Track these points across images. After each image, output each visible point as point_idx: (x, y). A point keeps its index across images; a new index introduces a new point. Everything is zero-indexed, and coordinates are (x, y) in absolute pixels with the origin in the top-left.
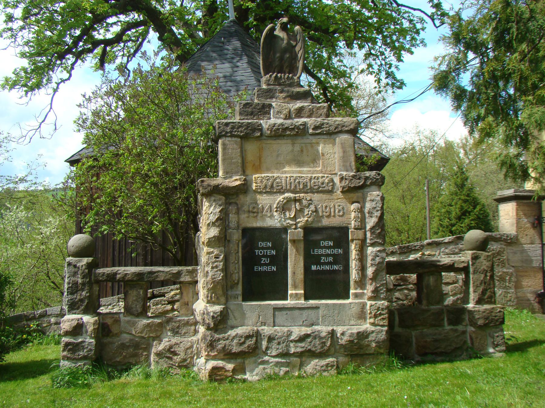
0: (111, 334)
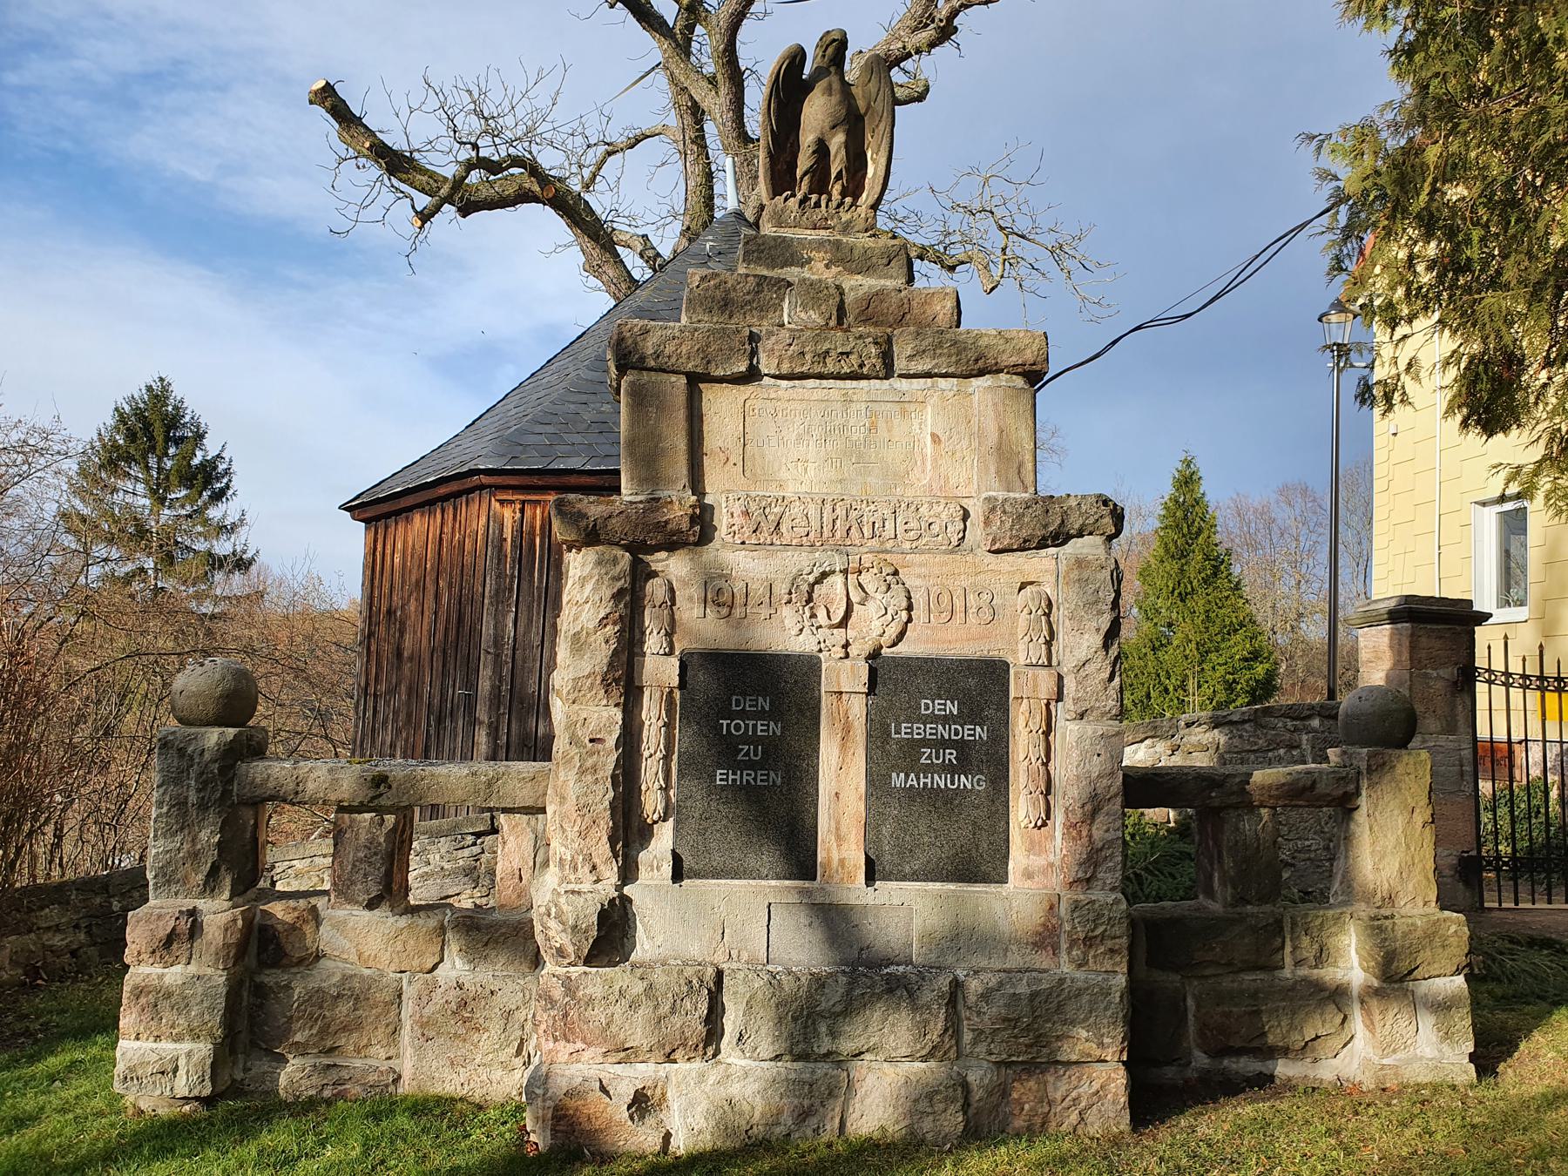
0: (284, 961)
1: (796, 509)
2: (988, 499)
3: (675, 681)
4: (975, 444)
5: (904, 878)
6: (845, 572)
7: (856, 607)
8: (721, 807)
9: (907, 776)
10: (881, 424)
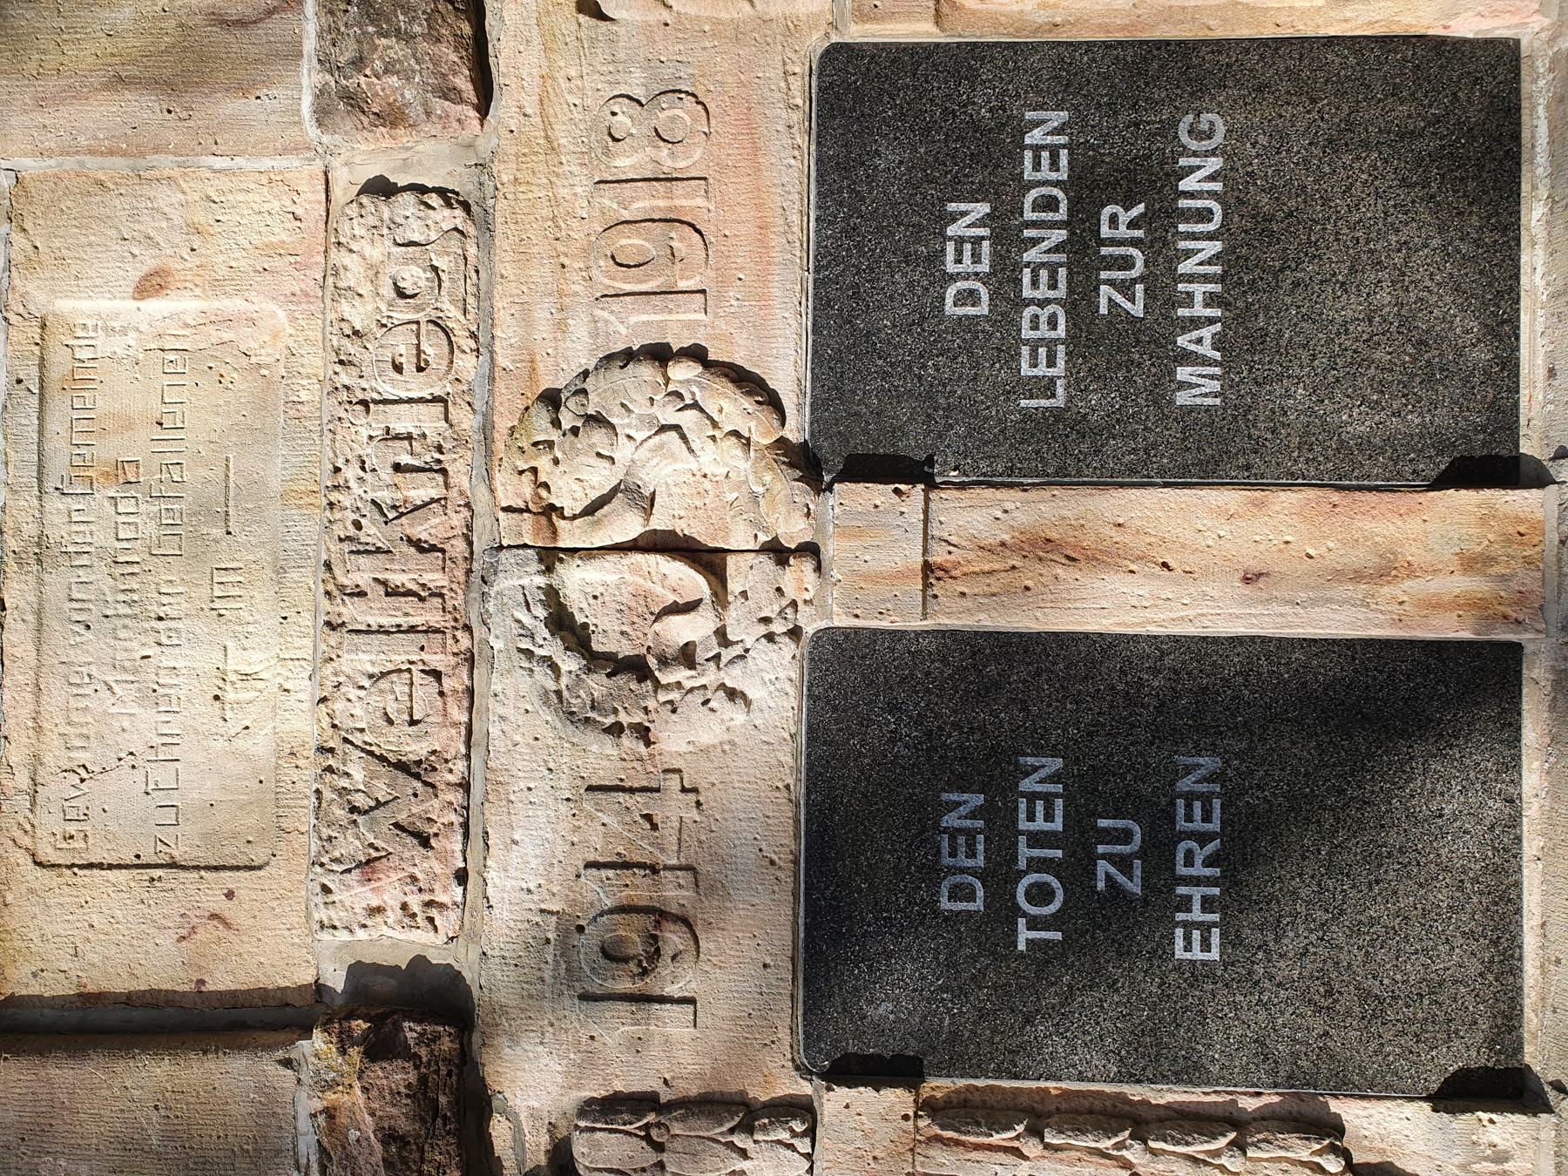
1: (357, 710)
2: (323, 115)
3: (897, 1099)
4: (165, 164)
5: (1509, 365)
6: (550, 557)
7: (659, 522)
8: (1290, 944)
9: (1187, 358)
10: (108, 450)
